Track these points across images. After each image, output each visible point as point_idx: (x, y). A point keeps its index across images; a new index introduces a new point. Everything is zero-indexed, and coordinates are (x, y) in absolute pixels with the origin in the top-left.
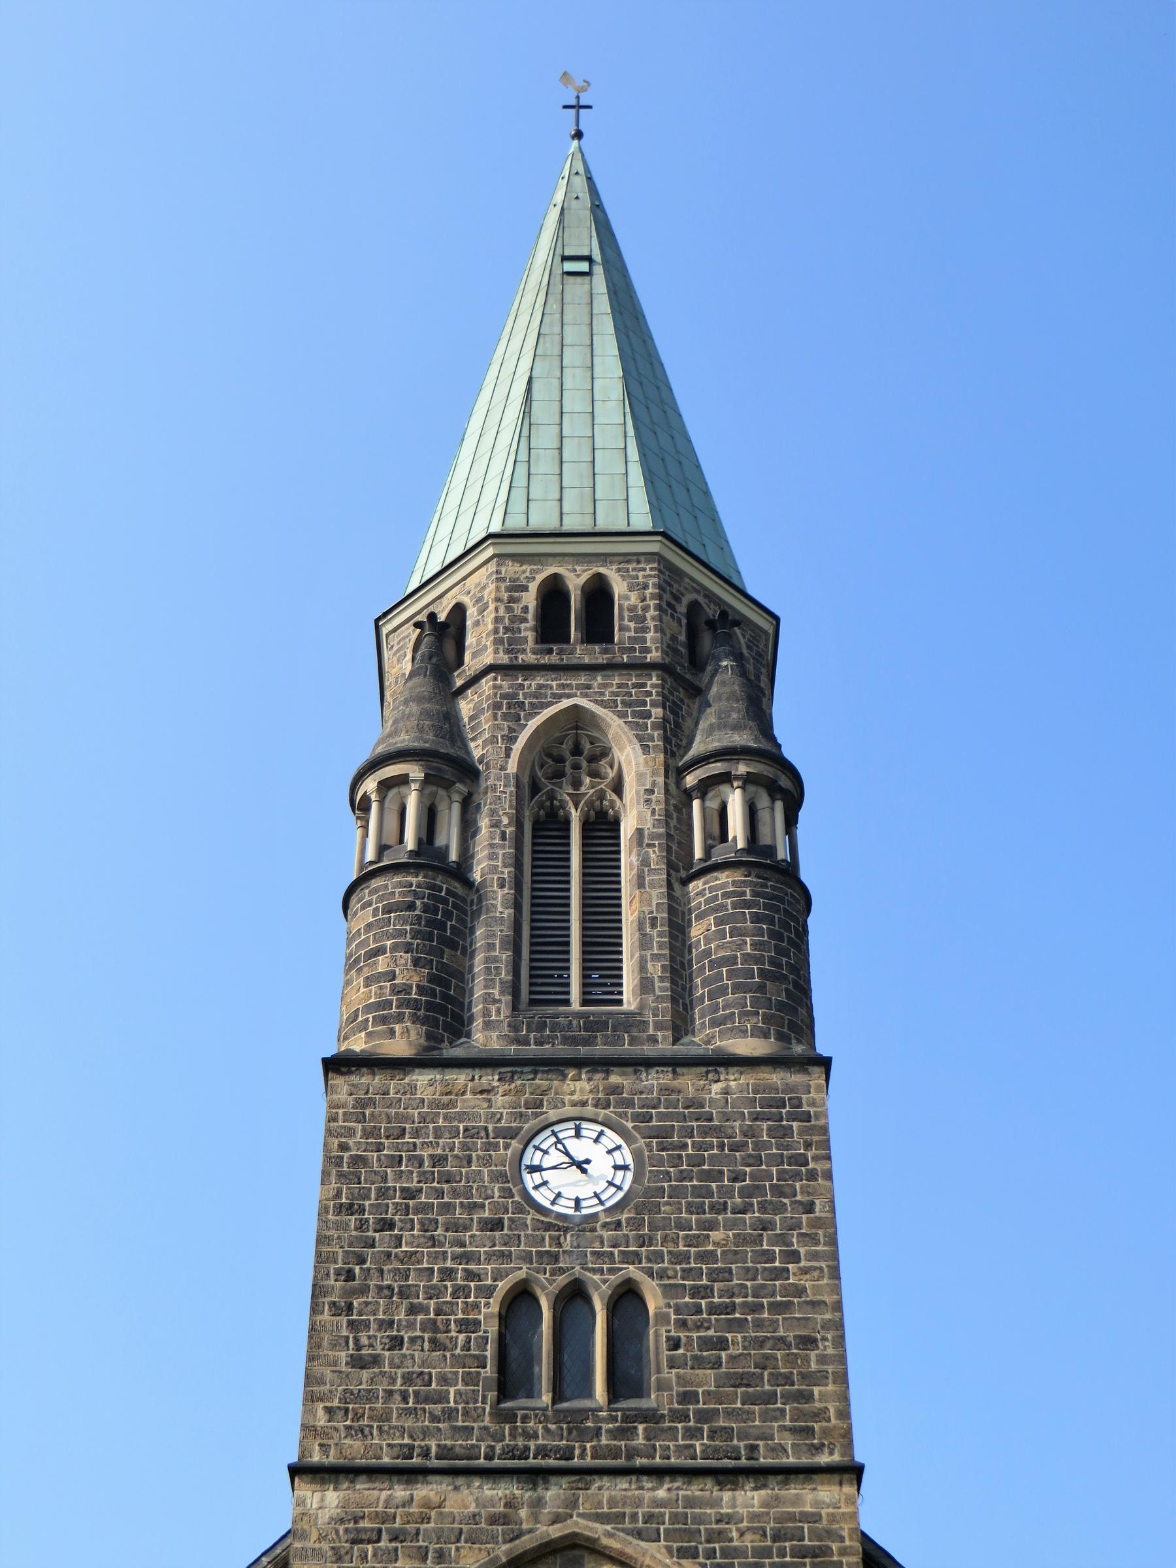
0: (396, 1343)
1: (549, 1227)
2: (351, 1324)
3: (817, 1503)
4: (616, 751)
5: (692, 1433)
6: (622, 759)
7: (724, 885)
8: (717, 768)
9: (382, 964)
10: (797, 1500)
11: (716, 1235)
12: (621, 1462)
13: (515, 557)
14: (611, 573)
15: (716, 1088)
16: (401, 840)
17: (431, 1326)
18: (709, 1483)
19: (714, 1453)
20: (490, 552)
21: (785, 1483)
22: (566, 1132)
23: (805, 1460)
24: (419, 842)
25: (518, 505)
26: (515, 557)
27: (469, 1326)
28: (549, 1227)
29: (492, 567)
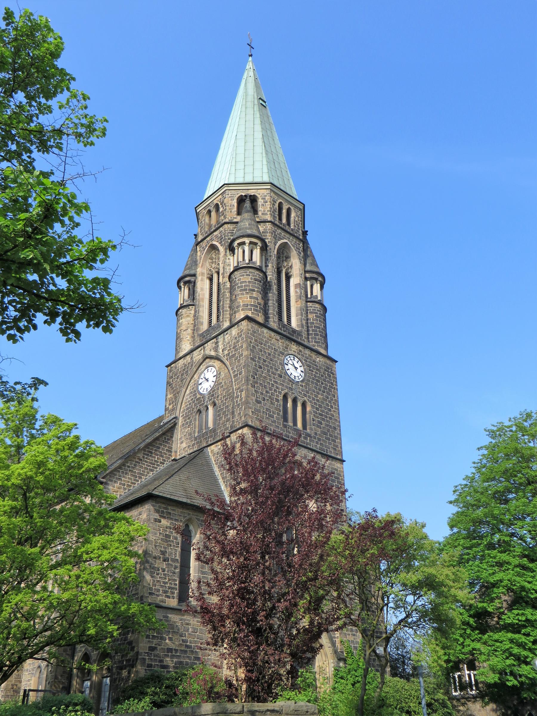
0: (264, 400)
1: (291, 381)
2: (255, 390)
3: (337, 467)
4: (292, 259)
5: (317, 443)
6: (293, 262)
7: (317, 308)
8: (315, 276)
9: (255, 294)
10: (334, 465)
11: (320, 396)
12: (305, 445)
13: (274, 192)
14: (292, 208)
15: (318, 359)
16: (244, 259)
17: (270, 397)
18: (320, 455)
19: (320, 449)
20: (269, 187)
21: (332, 460)
22: (296, 359)
23: (335, 456)
24: (249, 260)
25: (249, 169)
26: (274, 192)
27: (277, 400)
28: (291, 381)
29: (268, 191)
